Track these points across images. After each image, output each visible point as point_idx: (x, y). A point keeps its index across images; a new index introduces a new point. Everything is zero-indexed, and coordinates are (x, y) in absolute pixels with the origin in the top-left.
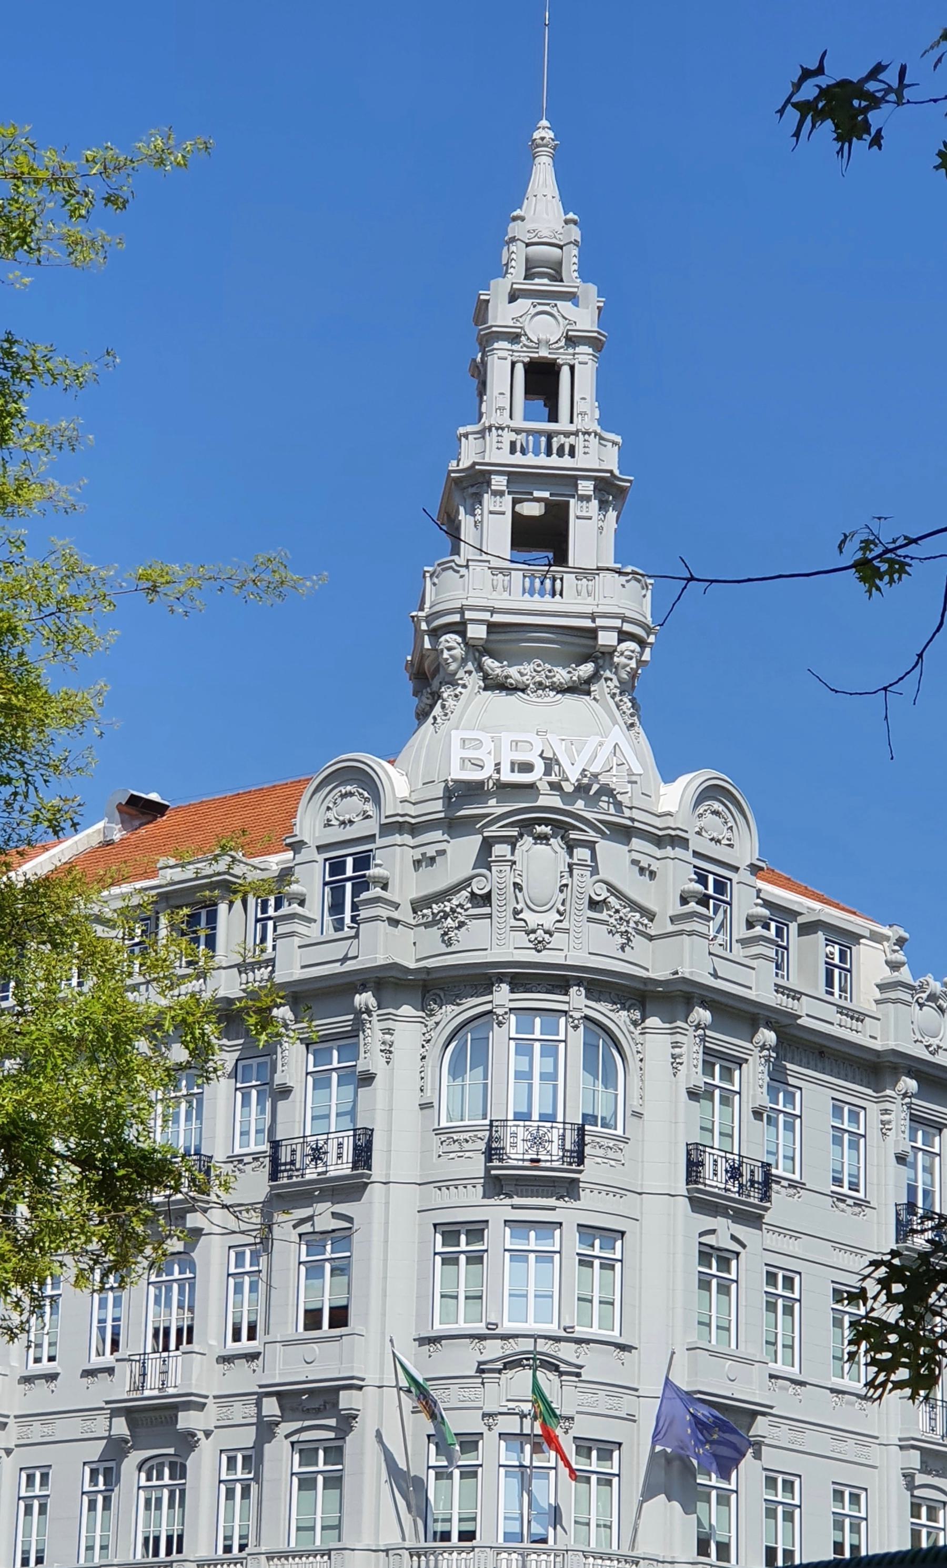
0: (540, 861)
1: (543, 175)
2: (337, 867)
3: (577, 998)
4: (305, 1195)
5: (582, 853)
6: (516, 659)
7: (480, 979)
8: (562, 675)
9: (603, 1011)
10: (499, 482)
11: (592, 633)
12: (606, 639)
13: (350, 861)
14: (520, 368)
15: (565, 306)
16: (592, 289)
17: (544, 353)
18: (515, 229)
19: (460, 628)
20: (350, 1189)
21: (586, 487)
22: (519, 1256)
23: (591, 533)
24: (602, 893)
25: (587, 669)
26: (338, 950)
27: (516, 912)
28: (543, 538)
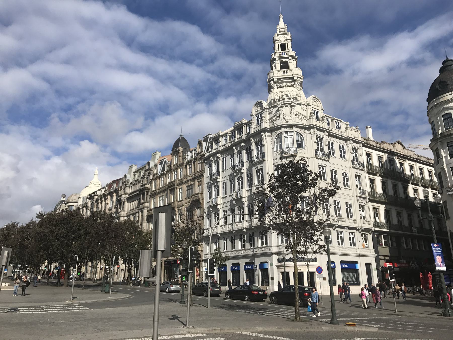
0: (286, 110)
1: (281, 20)
2: (258, 117)
3: (295, 129)
4: (256, 164)
5: (293, 107)
7: (279, 128)
8: (289, 84)
9: (299, 130)
10: (277, 59)
11: (293, 78)
12: (295, 78)
14: (280, 45)
15: (285, 35)
16: (289, 33)
17: (283, 42)
18: (278, 27)
19: (273, 80)
20: (262, 162)
21: (290, 58)
22: (286, 132)
23: (292, 64)
24: (297, 113)
25: (293, 83)
26: (259, 128)
28: (284, 66)
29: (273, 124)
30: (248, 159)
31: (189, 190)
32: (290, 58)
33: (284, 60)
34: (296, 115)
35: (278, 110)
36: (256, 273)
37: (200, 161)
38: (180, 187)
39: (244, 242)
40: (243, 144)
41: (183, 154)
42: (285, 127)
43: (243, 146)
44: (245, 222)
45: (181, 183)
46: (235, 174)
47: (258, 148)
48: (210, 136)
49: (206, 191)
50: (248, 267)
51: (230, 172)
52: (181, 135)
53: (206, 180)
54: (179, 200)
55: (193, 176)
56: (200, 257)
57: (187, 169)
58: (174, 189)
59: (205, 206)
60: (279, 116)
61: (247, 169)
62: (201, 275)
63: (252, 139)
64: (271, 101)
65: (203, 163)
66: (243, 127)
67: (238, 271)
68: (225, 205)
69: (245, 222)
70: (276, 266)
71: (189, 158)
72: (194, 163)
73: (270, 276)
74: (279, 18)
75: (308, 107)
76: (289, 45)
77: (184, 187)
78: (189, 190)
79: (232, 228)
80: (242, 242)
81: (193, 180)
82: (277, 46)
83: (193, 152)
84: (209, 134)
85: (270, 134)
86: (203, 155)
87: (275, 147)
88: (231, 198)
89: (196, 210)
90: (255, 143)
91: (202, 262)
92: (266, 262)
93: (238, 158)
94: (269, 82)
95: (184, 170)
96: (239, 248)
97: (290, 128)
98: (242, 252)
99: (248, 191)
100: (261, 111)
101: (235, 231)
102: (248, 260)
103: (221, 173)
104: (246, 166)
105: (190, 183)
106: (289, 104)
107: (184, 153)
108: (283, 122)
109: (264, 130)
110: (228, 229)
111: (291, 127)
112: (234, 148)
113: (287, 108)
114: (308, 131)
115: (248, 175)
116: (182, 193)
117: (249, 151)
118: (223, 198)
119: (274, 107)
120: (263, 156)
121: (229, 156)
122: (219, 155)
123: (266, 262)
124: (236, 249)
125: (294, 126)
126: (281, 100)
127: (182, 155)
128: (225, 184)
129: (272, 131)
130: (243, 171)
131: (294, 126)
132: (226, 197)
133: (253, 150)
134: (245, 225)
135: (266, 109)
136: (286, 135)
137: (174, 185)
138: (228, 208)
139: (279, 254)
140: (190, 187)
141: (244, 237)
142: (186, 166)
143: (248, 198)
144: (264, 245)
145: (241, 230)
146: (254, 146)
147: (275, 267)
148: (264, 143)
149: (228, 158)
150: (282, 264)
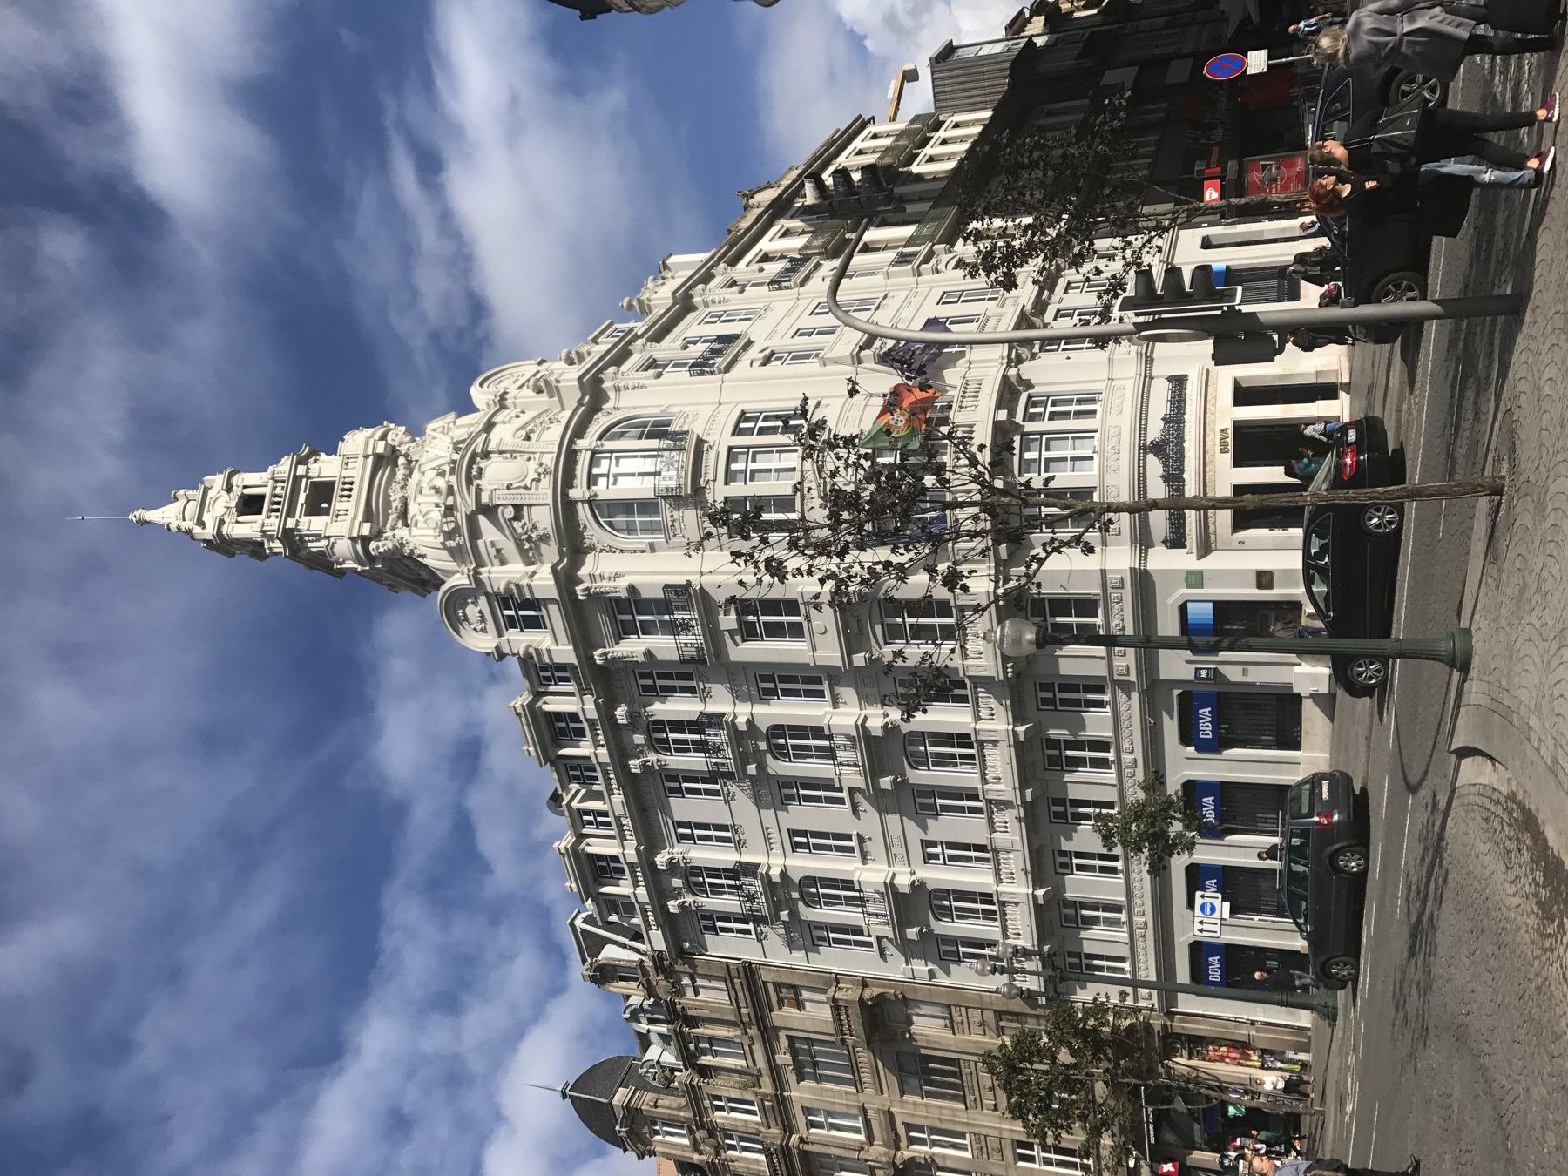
0: (496, 473)
1: (154, 516)
2: (511, 623)
4: (713, 634)
6: (387, 503)
7: (566, 509)
9: (595, 429)
10: (291, 523)
12: (380, 449)
13: (506, 612)
14: (241, 518)
15: (211, 494)
17: (233, 504)
19: (365, 541)
22: (592, 480)
23: (326, 467)
25: (401, 460)
27: (526, 488)
28: (321, 496)
29: (544, 538)
30: (692, 690)
31: (815, 1065)
32: (301, 470)
33: (302, 498)
34: (528, 438)
35: (490, 511)
36: (1234, 674)
37: (686, 981)
38: (800, 1121)
39: (1080, 745)
40: (621, 713)
41: (648, 1088)
42: (569, 480)
43: (630, 714)
44: (1001, 888)
45: (780, 1110)
46: (752, 769)
47: (647, 629)
48: (578, 922)
49: (829, 960)
50: (1206, 730)
51: (743, 808)
52: (564, 1095)
53: (774, 953)
54: (862, 1137)
55: (753, 1031)
56: (1148, 1026)
57: (719, 1070)
58: (805, 1155)
59: (897, 970)
60: (518, 508)
61: (738, 697)
62: (1241, 1033)
63: (597, 653)
64: (451, 551)
65: (693, 966)
66: (589, 850)
67: (1225, 792)
68: (898, 849)
69: (1001, 888)
70: (1200, 557)
71: (669, 1058)
72: (693, 1022)
73: (1251, 593)
74: (143, 522)
75: (508, 402)
76: (253, 481)
77: (801, 1093)
78: (815, 1065)
79: (1008, 804)
80: (1080, 762)
81: (769, 1034)
82: (246, 528)
83: (643, 1027)
84: (572, 924)
85: (590, 558)
86: (658, 958)
87: (642, 539)
88: (891, 950)
89: (914, 1029)
90: (619, 638)
91: (1171, 1015)
92: (1183, 609)
93: (718, 890)
94: (371, 559)
95: (725, 1087)
96: (1122, 934)
97: (575, 462)
98: (1138, 920)
99: (835, 702)
100: (483, 600)
101: (1022, 788)
102: (1171, 727)
103: (746, 858)
104: (722, 702)
105: (784, 1058)
106: (472, 461)
107: (642, 1085)
108: (545, 491)
109: (566, 579)
110: (1011, 834)
111: (572, 456)
112: (673, 906)
113: (487, 474)
114: (607, 399)
115: (766, 696)
116: (829, 1114)
117: (659, 678)
118: (864, 858)
119: (475, 533)
120: (680, 594)
121: (675, 802)
122: (661, 859)
123: (1183, 609)
124: (1124, 951)
125: (571, 442)
126: (450, 501)
127: (649, 1097)
128: (800, 840)
129: (574, 547)
130: (741, 721)
131: (571, 442)
132: (861, 839)
133: (649, 654)
134: (996, 722)
135: (476, 573)
136: (602, 482)
137: (785, 1150)
138: (915, 833)
139: (1143, 540)
140: (806, 1058)
141: (1054, 743)
142: (705, 1071)
143: (870, 704)
144: (1111, 756)
145: (1021, 750)
146: (633, 647)
147: (1210, 563)
148: (620, 587)
149: (684, 808)
150: (1191, 516)
